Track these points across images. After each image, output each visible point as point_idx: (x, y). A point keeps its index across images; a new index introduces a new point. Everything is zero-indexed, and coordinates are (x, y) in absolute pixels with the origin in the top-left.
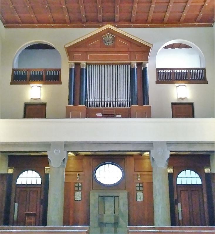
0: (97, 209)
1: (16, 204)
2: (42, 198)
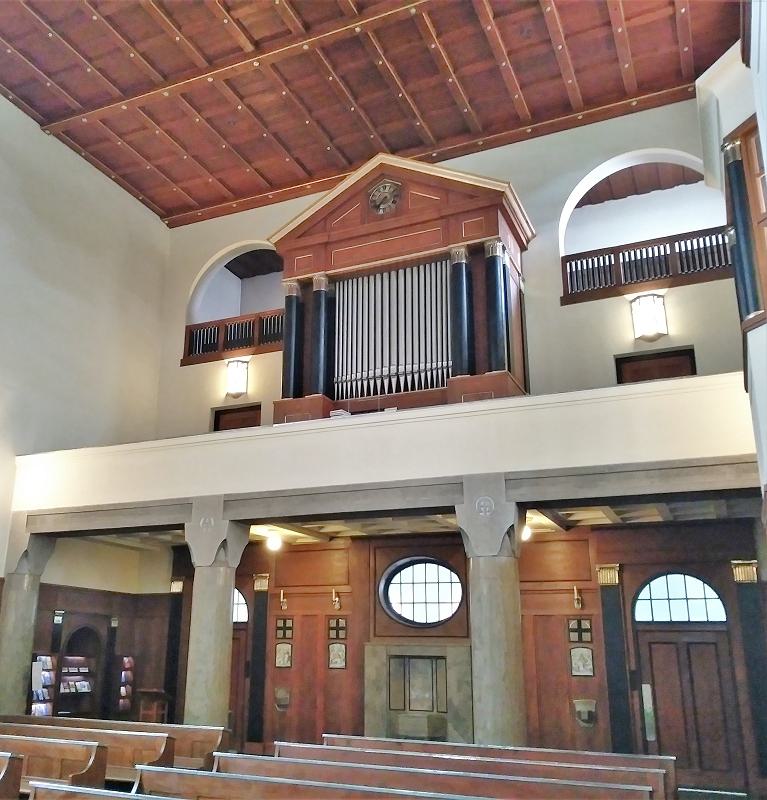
0: (384, 693)
2: (249, 658)
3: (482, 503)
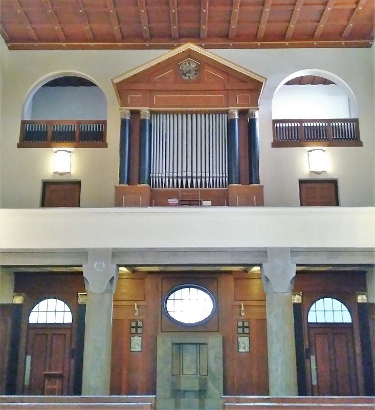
0: (170, 366)
1: (29, 358)
2: (73, 346)
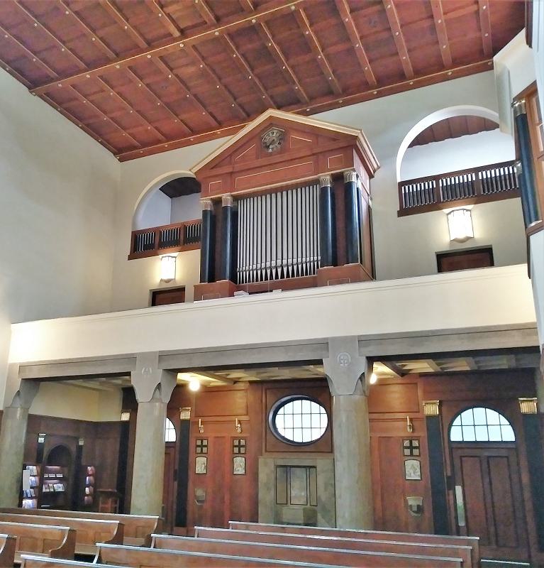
0: (273, 492)
2: (177, 467)
3: (342, 357)
